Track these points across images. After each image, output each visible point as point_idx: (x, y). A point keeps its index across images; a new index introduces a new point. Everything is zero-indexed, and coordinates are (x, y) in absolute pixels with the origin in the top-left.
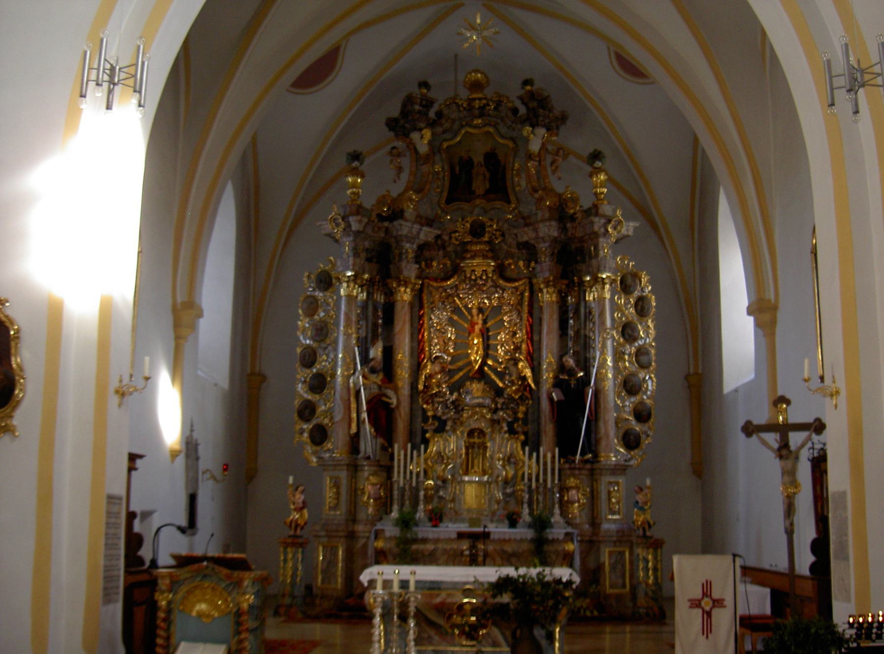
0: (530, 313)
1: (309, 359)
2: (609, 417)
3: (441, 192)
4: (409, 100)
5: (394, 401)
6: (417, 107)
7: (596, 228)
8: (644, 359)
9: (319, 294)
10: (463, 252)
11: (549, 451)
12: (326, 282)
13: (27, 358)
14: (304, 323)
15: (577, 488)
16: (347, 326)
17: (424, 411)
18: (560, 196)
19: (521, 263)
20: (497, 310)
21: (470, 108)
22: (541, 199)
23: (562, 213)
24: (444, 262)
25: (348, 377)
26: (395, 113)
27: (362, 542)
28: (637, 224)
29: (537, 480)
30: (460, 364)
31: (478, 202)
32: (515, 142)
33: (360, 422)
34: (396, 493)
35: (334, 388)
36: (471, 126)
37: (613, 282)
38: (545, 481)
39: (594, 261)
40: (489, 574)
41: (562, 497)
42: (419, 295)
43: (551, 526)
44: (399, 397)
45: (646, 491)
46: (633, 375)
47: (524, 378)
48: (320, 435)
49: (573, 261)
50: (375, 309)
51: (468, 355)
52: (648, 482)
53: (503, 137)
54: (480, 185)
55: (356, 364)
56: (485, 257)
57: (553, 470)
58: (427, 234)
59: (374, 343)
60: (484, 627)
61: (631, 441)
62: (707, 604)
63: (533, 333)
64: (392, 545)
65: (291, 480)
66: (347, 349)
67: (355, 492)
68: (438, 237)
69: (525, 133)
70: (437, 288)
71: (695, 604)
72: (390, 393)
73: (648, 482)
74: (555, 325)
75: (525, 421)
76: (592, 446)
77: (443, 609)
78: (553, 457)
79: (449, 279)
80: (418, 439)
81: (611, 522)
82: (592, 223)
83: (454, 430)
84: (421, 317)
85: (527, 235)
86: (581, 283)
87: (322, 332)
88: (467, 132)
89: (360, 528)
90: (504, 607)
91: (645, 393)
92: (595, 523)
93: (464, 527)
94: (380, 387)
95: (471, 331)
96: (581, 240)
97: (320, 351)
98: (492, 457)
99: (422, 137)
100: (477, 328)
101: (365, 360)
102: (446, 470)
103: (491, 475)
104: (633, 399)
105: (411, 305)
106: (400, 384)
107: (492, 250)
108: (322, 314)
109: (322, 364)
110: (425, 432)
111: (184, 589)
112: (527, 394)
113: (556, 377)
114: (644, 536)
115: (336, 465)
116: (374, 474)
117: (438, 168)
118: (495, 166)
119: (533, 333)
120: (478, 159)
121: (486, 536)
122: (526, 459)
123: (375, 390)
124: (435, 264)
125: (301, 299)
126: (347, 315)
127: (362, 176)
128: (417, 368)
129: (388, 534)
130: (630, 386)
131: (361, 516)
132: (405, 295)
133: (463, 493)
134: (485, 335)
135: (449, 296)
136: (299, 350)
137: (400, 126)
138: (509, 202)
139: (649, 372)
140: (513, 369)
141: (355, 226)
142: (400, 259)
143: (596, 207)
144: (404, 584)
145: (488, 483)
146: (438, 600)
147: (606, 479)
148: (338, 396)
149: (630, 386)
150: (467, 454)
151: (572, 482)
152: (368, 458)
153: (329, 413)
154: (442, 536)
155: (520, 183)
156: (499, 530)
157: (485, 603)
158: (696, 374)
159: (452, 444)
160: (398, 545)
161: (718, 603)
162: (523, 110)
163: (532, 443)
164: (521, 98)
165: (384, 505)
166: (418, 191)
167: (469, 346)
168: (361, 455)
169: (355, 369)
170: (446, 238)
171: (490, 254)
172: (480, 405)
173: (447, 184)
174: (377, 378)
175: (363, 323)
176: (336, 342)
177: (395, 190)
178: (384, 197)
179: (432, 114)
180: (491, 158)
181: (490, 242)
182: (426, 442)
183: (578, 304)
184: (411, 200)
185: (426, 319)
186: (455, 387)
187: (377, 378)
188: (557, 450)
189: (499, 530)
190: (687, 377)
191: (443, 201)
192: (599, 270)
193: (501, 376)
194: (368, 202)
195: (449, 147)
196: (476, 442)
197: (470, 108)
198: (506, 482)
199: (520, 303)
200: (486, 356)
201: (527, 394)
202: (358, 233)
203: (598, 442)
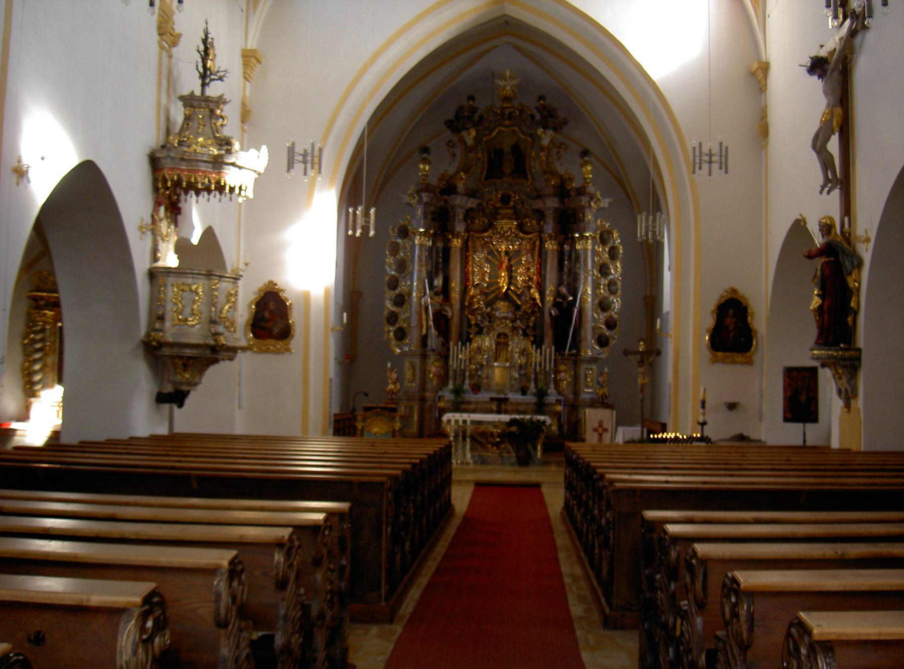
0: (540, 256)
1: (394, 284)
2: (588, 326)
3: (481, 173)
4: (460, 109)
5: (450, 314)
6: (466, 114)
7: (583, 203)
8: (613, 288)
9: (399, 241)
10: (494, 215)
11: (548, 348)
12: (404, 233)
13: (295, 318)
14: (390, 260)
15: (566, 371)
16: (420, 266)
17: (469, 320)
18: (561, 177)
19: (534, 222)
20: (518, 253)
21: (502, 113)
22: (548, 180)
23: (563, 191)
24: (482, 221)
25: (421, 298)
26: (451, 116)
27: (429, 403)
28: (611, 200)
29: (540, 365)
30: (493, 289)
31: (506, 179)
32: (532, 138)
33: (428, 328)
34: (451, 373)
35: (411, 304)
36: (502, 126)
37: (594, 238)
38: (545, 366)
39: (582, 225)
40: (506, 418)
41: (556, 377)
42: (466, 243)
43: (547, 395)
44: (453, 311)
45: (605, 375)
46: (606, 298)
47: (534, 299)
48: (401, 335)
49: (568, 223)
50: (437, 252)
51: (498, 283)
52: (606, 370)
53: (524, 134)
54: (508, 168)
55: (425, 288)
56: (510, 218)
57: (550, 360)
58: (471, 203)
59: (437, 275)
60: (504, 443)
61: (602, 341)
62: (600, 430)
63: (541, 273)
64: (449, 405)
65: (389, 365)
66: (420, 280)
67: (424, 372)
68: (479, 204)
69: (539, 133)
70: (478, 238)
71: (595, 430)
72: (448, 309)
73: (606, 370)
74: (555, 265)
75: (534, 328)
76: (577, 344)
77: (483, 434)
78: (551, 352)
79: (485, 231)
80: (465, 337)
81: (587, 393)
82: (581, 200)
83: (488, 333)
84: (467, 257)
85: (538, 205)
86: (573, 238)
87: (402, 266)
88: (501, 131)
89: (428, 395)
90: (512, 433)
91: (613, 310)
92: (576, 393)
93: (495, 395)
94: (441, 304)
95: (500, 267)
96: (574, 209)
97: (401, 279)
98: (512, 351)
99: (469, 134)
100: (504, 265)
101: (431, 286)
102: (483, 358)
103: (511, 362)
104: (605, 314)
105: (461, 249)
106: (454, 302)
107: (515, 213)
108: (402, 255)
109: (403, 287)
110: (469, 334)
111: (369, 421)
112: (536, 309)
113: (555, 300)
114: (603, 402)
115: (412, 354)
116: (437, 360)
117: (480, 155)
118: (519, 154)
119: (541, 273)
120: (507, 149)
121: (507, 399)
122: (534, 352)
123: (438, 307)
124: (477, 221)
125: (388, 244)
126: (420, 257)
127: (429, 163)
128: (465, 291)
129: (446, 398)
130: (603, 306)
131: (429, 386)
132: (457, 243)
133: (493, 372)
134: (510, 270)
135: (486, 243)
136: (387, 279)
137: (456, 124)
138: (527, 180)
139: (617, 297)
140: (527, 293)
141: (425, 199)
142: (454, 220)
143: (584, 187)
144: (465, 422)
145: (510, 367)
146: (481, 430)
147: (583, 366)
148: (413, 310)
149: (603, 306)
150: (496, 348)
151: (562, 367)
152: (433, 350)
153: (408, 320)
154: (480, 400)
155: (535, 167)
156: (515, 397)
157: (504, 430)
158: (651, 296)
159: (487, 342)
160: (453, 405)
161: (606, 430)
162: (538, 117)
163: (538, 342)
164: (537, 108)
165: (443, 380)
166: (466, 172)
167: (499, 277)
168: (429, 348)
169: (425, 293)
170: (484, 204)
171: (514, 217)
172: (506, 318)
173: (486, 166)
174: (440, 299)
175: (430, 262)
176: (412, 273)
177: (451, 171)
178: (443, 175)
179: (476, 118)
180: (517, 149)
181: (514, 208)
182: (470, 340)
183: (571, 251)
184: (462, 179)
185: (470, 258)
186: (488, 304)
187: (440, 299)
188: (553, 348)
189: (515, 397)
190: (645, 298)
191: (483, 178)
192: (585, 231)
193: (519, 296)
194: (434, 181)
195: (487, 141)
196: (502, 342)
197: (502, 113)
198: (521, 367)
199: (533, 249)
200: (509, 284)
201: (536, 309)
202: (426, 204)
203: (580, 341)
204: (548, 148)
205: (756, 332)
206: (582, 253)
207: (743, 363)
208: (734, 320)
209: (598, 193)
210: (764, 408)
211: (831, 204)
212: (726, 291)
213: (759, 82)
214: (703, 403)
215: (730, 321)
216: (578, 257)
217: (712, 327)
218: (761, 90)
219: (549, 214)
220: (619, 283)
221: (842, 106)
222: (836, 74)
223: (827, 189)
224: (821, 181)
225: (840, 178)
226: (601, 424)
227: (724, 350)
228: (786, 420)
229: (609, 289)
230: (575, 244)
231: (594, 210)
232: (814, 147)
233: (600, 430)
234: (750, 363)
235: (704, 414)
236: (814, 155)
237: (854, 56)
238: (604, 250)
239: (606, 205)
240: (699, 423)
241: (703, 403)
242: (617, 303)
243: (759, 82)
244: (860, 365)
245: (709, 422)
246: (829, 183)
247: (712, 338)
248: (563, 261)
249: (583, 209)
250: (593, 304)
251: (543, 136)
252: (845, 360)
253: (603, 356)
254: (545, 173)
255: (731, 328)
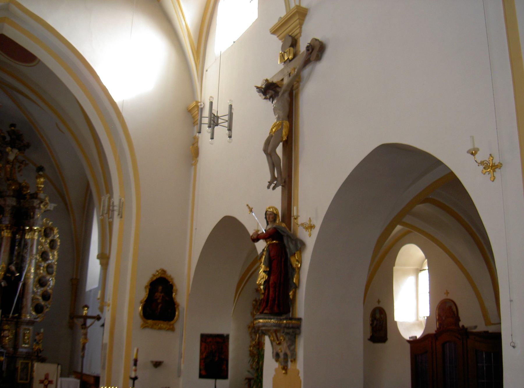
2: (29, 296)
7: (35, 204)
8: (50, 270)
15: (9, 330)
18: (20, 184)
22: (10, 185)
23: (20, 194)
28: (56, 205)
37: (40, 231)
39: (32, 220)
45: (41, 335)
46: (44, 277)
49: (22, 218)
52: (42, 330)
61: (38, 309)
71: (42, 382)
74: (8, 248)
76: (19, 309)
82: (33, 202)
86: (24, 230)
92: (16, 347)
104: (42, 289)
113: (5, 275)
130: (41, 282)
139: (52, 277)
162: (8, 139)
164: (8, 132)
190: (72, 279)
192: (34, 225)
203: (22, 308)
204: (13, 162)
205: (178, 306)
206: (29, 241)
207: (169, 329)
208: (162, 294)
209: (47, 199)
210: (182, 366)
211: (275, 199)
212: (157, 271)
213: (193, 118)
214: (136, 361)
215: (159, 295)
216: (26, 244)
217: (145, 299)
218: (194, 123)
219: (8, 209)
220: (55, 267)
221: (289, 121)
222: (286, 95)
223: (273, 185)
224: (269, 178)
225: (284, 176)
226: (47, 377)
227: (153, 319)
228: (201, 376)
229: (47, 271)
230: (25, 234)
231: (43, 211)
232: (265, 151)
233: (46, 382)
234: (173, 329)
235: (135, 370)
236: (264, 156)
237: (301, 84)
238: (46, 242)
239: (52, 209)
240: (131, 378)
241: (136, 361)
242: (52, 282)
243: (193, 118)
244: (299, 333)
245: (139, 376)
246: (273, 183)
247: (144, 308)
248: (15, 246)
249: (34, 208)
250: (34, 281)
251: (10, 153)
252: (289, 328)
253: (38, 320)
254: (8, 180)
255: (159, 301)
